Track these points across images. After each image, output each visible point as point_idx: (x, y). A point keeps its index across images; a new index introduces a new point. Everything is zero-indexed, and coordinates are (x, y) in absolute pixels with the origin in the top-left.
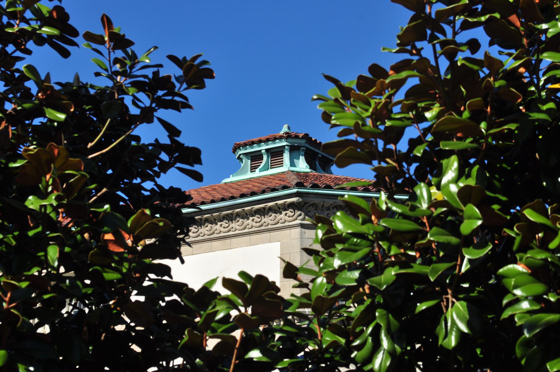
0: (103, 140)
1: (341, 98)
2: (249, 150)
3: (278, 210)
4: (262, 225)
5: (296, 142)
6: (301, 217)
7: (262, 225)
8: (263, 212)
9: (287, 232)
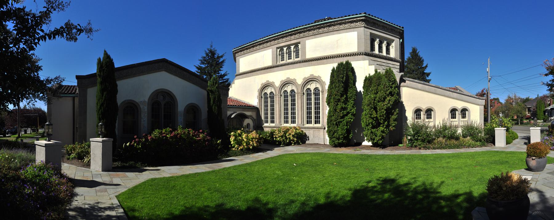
1: (198, 70)
3: (356, 21)
4: (324, 31)
6: (364, 24)
8: (351, 22)
9: (360, 28)
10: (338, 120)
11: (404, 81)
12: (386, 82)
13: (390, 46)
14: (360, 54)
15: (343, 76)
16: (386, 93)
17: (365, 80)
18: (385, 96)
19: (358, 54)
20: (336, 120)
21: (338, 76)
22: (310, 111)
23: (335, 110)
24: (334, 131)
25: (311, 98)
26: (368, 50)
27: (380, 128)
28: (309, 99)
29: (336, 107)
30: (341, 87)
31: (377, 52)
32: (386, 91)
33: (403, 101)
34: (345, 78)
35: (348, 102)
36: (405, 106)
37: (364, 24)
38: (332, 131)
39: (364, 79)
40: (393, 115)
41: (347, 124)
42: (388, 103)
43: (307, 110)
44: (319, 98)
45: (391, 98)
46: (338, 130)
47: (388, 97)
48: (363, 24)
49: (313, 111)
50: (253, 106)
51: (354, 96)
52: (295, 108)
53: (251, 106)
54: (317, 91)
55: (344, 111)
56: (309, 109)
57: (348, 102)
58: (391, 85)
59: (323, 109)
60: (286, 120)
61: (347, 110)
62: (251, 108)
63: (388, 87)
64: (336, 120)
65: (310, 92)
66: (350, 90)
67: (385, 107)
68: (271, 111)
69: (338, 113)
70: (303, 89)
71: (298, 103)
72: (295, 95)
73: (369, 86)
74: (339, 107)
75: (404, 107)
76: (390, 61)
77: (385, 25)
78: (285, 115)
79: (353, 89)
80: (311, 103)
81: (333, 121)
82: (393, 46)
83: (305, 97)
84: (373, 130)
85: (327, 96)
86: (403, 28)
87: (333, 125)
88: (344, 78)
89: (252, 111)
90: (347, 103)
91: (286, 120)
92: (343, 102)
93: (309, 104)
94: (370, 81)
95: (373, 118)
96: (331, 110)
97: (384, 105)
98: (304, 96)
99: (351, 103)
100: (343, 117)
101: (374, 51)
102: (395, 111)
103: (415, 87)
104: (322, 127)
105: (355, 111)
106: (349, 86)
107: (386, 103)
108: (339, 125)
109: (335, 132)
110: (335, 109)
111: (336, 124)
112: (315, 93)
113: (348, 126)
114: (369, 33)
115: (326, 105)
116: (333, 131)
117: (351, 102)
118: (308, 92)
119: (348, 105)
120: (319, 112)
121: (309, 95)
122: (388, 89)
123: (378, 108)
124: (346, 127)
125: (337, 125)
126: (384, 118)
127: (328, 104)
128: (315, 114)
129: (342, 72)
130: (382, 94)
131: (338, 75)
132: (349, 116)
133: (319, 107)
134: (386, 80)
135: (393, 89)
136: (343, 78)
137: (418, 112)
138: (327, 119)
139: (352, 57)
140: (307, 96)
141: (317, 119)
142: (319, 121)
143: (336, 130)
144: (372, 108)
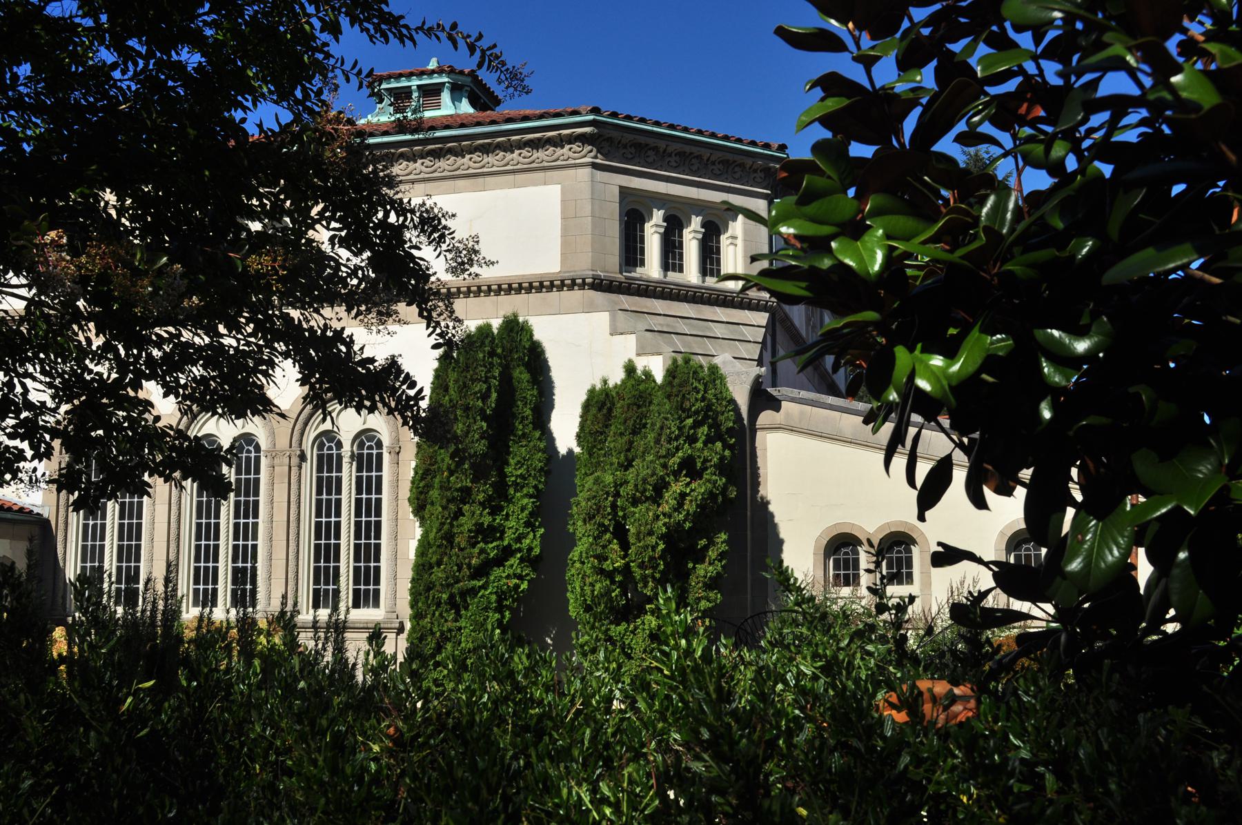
0: (289, 36)
2: (394, 85)
3: (558, 142)
5: (461, 80)
6: (592, 154)
7: (435, 171)
8: (536, 145)
9: (572, 172)
10: (457, 581)
11: (775, 405)
12: (667, 419)
13: (723, 238)
14: (573, 285)
15: (485, 386)
16: (665, 466)
17: (586, 407)
18: (662, 478)
19: (563, 284)
20: (448, 585)
21: (464, 388)
22: (333, 541)
23: (449, 538)
24: (442, 633)
25: (339, 480)
26: (611, 266)
27: (643, 623)
28: (328, 485)
29: (451, 525)
30: (477, 436)
31: (652, 268)
32: (664, 457)
33: (770, 497)
34: (494, 395)
35: (509, 501)
36: (777, 520)
37: (592, 154)
38: (433, 634)
39: (585, 397)
40: (703, 562)
41: (500, 601)
42: (676, 510)
43: (318, 537)
44: (379, 479)
45: (688, 485)
46: (460, 629)
47: (677, 480)
48: (587, 154)
49: (346, 542)
50: (21, 510)
51: (535, 477)
52: (256, 525)
53: (10, 509)
54: (370, 448)
55: (486, 543)
56: (326, 531)
57: (509, 501)
58: (691, 428)
59: (395, 537)
60: (201, 587)
61: (501, 538)
62: (9, 516)
63: (677, 439)
64: (448, 585)
65: (334, 452)
66: (519, 451)
67: (660, 527)
68: (121, 538)
69: (461, 550)
70: (302, 434)
71: (272, 502)
72: (258, 459)
73: (601, 433)
74: (466, 523)
75: (775, 526)
76: (718, 309)
77: (695, 150)
78: (197, 560)
79: (532, 444)
80: (339, 502)
81: (438, 588)
82: (735, 238)
83: (309, 471)
84: (616, 630)
85: (416, 473)
86: (782, 148)
87: (439, 605)
88: (489, 397)
89: (13, 537)
90: (501, 509)
91: (201, 587)
92: (482, 504)
93: (327, 507)
94: (605, 411)
95: (610, 575)
96: (432, 536)
97: (657, 518)
98: (306, 467)
99: (523, 509)
100: (481, 571)
101: (642, 264)
102: (711, 543)
103: (828, 430)
104: (388, 620)
105: (537, 542)
106: (512, 430)
107: (667, 509)
108: (466, 609)
109: (445, 638)
110: (446, 533)
111: (452, 602)
112: (360, 456)
113: (507, 614)
114: (617, 191)
115: (411, 516)
116: (438, 634)
117: (522, 502)
118: (325, 452)
119: (507, 517)
120: (378, 547)
121: (328, 463)
122: (677, 449)
123: (633, 530)
124: (497, 616)
125: (456, 605)
126: (658, 576)
127: (420, 506)
128: (357, 559)
129: (482, 371)
130: (649, 471)
131: (465, 385)
132: (512, 566)
133: (378, 524)
134: (667, 407)
135: (699, 445)
136: (485, 397)
137: (843, 550)
138: (413, 581)
139: (534, 297)
140: (320, 470)
141: (367, 583)
142: (377, 592)
143: (450, 630)
144: (606, 530)
